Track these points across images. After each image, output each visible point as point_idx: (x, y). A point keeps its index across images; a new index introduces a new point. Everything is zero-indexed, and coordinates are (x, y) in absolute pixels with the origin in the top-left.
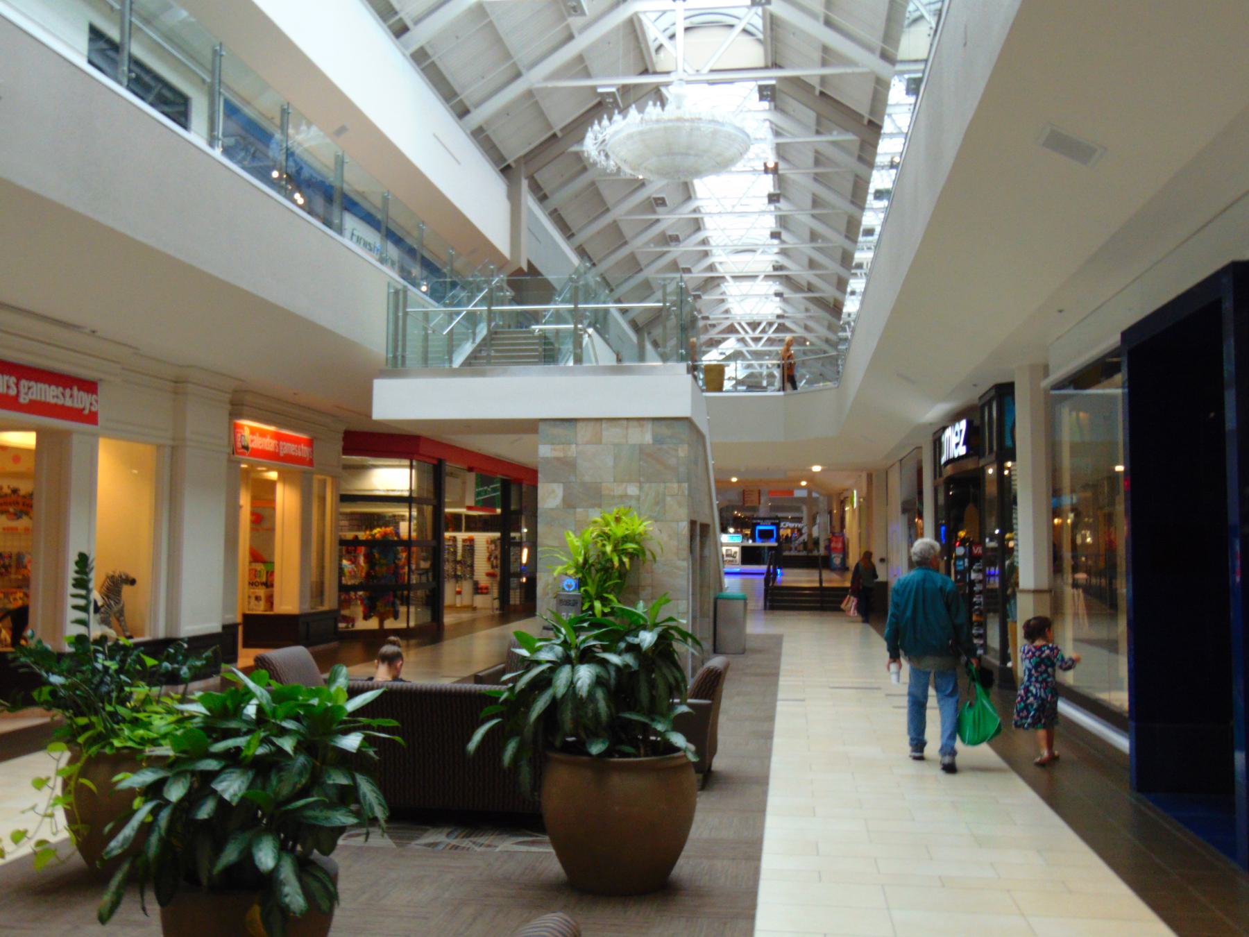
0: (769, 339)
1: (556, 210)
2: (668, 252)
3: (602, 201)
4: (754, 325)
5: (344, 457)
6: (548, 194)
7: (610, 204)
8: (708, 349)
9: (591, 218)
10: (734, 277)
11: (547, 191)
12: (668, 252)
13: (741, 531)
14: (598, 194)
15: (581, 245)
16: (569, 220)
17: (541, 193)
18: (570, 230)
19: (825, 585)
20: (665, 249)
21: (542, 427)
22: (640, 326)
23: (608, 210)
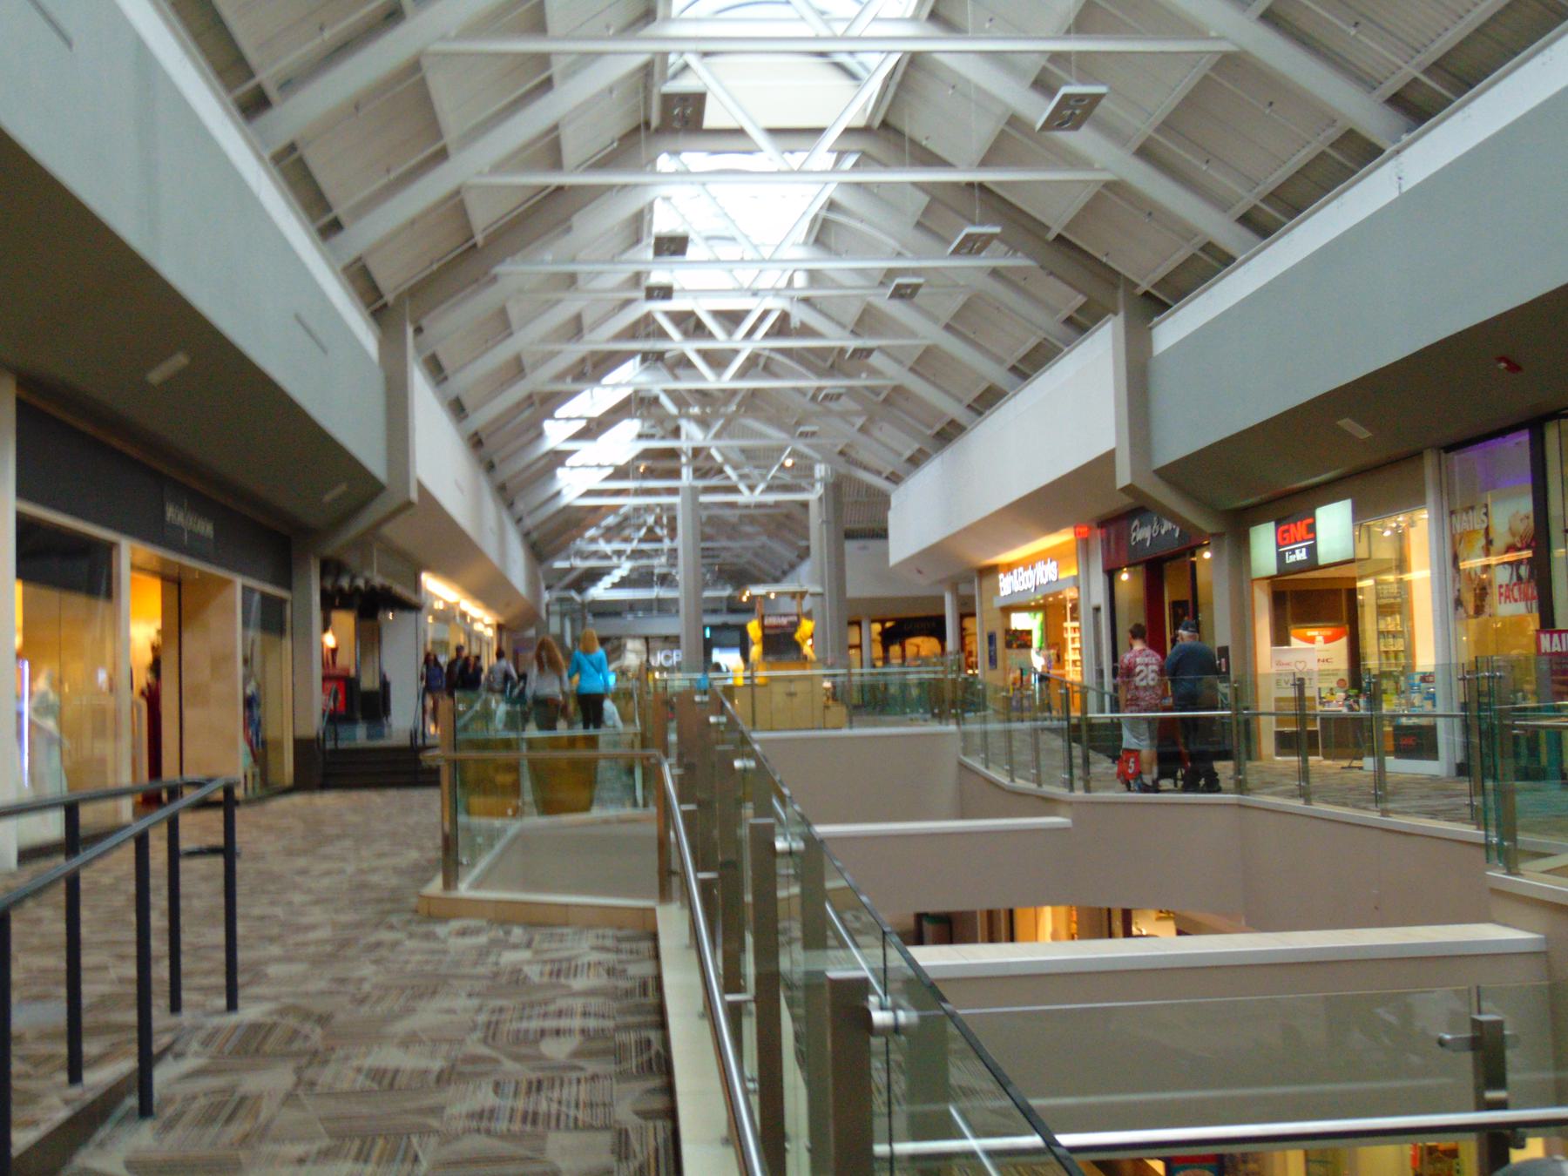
0: (753, 360)
1: (292, 148)
2: (559, 353)
3: (433, 128)
4: (731, 319)
5: (1279, 758)
6: (343, 219)
7: (450, 137)
8: (576, 387)
9: (393, 175)
10: (774, 132)
11: (340, 211)
12: (559, 353)
13: (812, 636)
14: (424, 100)
15: (359, 259)
16: (327, 180)
17: (327, 219)
18: (327, 208)
19: (877, 1042)
20: (557, 347)
21: (521, 671)
22: (389, 298)
23: (442, 155)
